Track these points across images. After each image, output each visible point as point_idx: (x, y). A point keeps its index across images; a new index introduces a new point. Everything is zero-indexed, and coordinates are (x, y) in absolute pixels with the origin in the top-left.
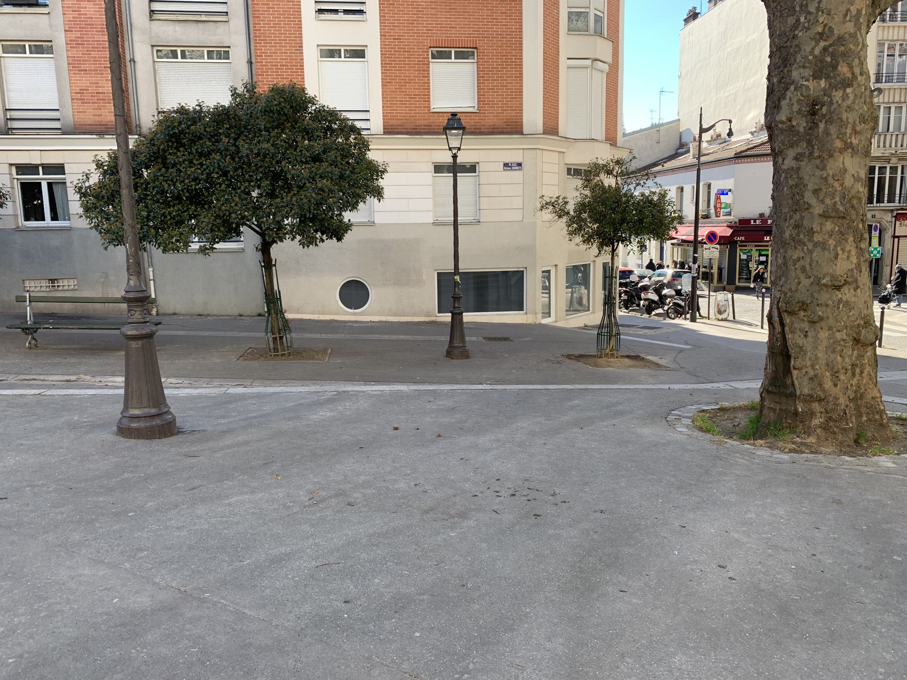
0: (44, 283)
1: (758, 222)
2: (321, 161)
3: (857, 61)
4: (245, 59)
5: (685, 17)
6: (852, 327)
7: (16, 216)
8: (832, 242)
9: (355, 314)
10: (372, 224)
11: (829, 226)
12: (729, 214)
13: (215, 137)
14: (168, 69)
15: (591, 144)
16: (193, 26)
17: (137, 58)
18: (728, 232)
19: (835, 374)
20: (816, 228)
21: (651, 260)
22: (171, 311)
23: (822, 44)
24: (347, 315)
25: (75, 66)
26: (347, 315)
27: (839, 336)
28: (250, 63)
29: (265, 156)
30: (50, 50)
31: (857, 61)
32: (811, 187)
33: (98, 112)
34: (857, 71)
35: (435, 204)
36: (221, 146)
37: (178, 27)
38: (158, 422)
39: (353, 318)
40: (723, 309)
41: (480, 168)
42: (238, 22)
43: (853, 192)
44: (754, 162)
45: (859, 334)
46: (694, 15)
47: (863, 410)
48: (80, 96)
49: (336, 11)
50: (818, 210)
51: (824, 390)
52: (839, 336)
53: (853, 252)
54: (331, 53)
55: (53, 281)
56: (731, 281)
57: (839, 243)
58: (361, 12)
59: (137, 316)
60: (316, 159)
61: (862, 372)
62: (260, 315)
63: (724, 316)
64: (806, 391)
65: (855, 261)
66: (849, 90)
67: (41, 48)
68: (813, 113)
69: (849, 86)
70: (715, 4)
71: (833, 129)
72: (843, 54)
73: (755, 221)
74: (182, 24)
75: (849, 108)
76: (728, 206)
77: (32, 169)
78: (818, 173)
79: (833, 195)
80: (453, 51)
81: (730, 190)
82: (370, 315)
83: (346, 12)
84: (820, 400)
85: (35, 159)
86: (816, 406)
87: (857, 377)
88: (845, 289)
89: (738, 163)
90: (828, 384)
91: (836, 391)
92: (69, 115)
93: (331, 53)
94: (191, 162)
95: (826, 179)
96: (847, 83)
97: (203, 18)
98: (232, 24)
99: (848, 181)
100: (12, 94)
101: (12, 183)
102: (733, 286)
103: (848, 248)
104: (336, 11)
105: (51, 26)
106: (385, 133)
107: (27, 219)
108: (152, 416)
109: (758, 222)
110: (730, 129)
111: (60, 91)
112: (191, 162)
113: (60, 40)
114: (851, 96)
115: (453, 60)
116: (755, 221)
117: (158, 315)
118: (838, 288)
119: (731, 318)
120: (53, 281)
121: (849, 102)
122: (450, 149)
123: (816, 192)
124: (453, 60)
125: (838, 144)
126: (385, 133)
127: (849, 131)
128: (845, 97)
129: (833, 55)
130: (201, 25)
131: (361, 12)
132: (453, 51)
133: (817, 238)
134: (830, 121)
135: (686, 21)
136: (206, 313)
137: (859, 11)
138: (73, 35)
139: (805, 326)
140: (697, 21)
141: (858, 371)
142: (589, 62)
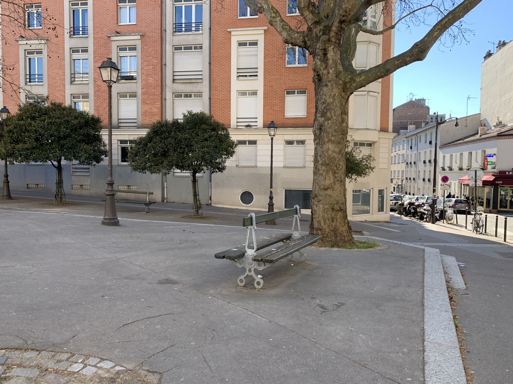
0: (126, 187)
1: (511, 173)
2: (207, 141)
3: (333, 111)
4: (208, 97)
5: (485, 55)
6: (331, 204)
7: (118, 160)
8: (324, 174)
9: (247, 207)
10: (256, 167)
11: (323, 168)
12: (494, 168)
13: (170, 132)
14: (178, 102)
15: (366, 131)
16: (188, 85)
17: (167, 98)
18: (492, 178)
19: (325, 220)
20: (320, 169)
21: (450, 193)
22: (172, 201)
23: (324, 105)
24: (243, 207)
25: (144, 102)
26: (243, 207)
27: (326, 207)
28: (210, 99)
29: (186, 139)
30: (135, 96)
31: (333, 111)
32: (319, 154)
33: (150, 120)
34: (333, 115)
35: (285, 159)
36: (171, 135)
37: (183, 85)
38: (112, 221)
39: (245, 208)
40: (450, 218)
41: (306, 142)
42: (206, 82)
43: (332, 156)
44: (509, 138)
45: (334, 206)
46: (489, 55)
47: (338, 235)
48: (144, 114)
49: (246, 76)
50: (320, 162)
51: (321, 226)
52: (326, 207)
53: (332, 178)
54: (243, 93)
55: (129, 186)
56: (495, 207)
57: (327, 174)
58: (257, 75)
59: (110, 188)
60: (206, 140)
61: (337, 221)
62: (207, 205)
63: (451, 222)
64: (316, 226)
65: (332, 180)
66: (329, 121)
67: (133, 95)
68: (320, 129)
69: (329, 120)
70: (500, 49)
71: (325, 135)
72: (329, 109)
73: (509, 172)
74: (184, 84)
75: (330, 128)
76: (493, 163)
77: (125, 142)
78: (321, 149)
79: (325, 157)
80: (296, 91)
81: (495, 154)
82: (253, 207)
83: (250, 76)
84: (320, 230)
85: (126, 138)
86: (319, 231)
87: (335, 222)
88: (329, 190)
89: (499, 139)
90: (323, 224)
91: (325, 227)
92: (140, 121)
93: (243, 93)
94: (161, 141)
95: (323, 152)
96: (329, 119)
97: (193, 81)
98: (203, 83)
99: (330, 152)
100: (121, 113)
101: (118, 147)
102: (495, 210)
103: (330, 176)
104: (246, 76)
105: (137, 87)
106: (264, 127)
107: (122, 161)
108: (111, 219)
109: (511, 173)
110: (457, 123)
111: (138, 111)
112: (161, 141)
113: (139, 92)
114: (330, 124)
115: (296, 94)
116: (509, 172)
117: (167, 202)
118: (326, 190)
119: (455, 223)
120: (129, 186)
121: (329, 125)
122: (270, 135)
123: (320, 156)
124: (296, 94)
125: (326, 140)
126: (264, 127)
127: (330, 135)
128: (328, 124)
129: (326, 109)
130: (192, 84)
131: (257, 75)
132: (296, 91)
133: (320, 172)
134: (324, 132)
135: (485, 58)
136: (186, 202)
137: (335, 95)
138: (144, 90)
139: (317, 203)
140: (491, 57)
141: (335, 220)
142: (366, 93)
